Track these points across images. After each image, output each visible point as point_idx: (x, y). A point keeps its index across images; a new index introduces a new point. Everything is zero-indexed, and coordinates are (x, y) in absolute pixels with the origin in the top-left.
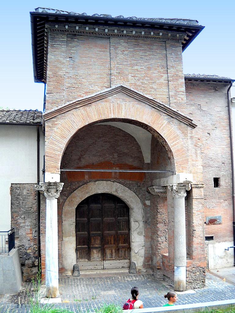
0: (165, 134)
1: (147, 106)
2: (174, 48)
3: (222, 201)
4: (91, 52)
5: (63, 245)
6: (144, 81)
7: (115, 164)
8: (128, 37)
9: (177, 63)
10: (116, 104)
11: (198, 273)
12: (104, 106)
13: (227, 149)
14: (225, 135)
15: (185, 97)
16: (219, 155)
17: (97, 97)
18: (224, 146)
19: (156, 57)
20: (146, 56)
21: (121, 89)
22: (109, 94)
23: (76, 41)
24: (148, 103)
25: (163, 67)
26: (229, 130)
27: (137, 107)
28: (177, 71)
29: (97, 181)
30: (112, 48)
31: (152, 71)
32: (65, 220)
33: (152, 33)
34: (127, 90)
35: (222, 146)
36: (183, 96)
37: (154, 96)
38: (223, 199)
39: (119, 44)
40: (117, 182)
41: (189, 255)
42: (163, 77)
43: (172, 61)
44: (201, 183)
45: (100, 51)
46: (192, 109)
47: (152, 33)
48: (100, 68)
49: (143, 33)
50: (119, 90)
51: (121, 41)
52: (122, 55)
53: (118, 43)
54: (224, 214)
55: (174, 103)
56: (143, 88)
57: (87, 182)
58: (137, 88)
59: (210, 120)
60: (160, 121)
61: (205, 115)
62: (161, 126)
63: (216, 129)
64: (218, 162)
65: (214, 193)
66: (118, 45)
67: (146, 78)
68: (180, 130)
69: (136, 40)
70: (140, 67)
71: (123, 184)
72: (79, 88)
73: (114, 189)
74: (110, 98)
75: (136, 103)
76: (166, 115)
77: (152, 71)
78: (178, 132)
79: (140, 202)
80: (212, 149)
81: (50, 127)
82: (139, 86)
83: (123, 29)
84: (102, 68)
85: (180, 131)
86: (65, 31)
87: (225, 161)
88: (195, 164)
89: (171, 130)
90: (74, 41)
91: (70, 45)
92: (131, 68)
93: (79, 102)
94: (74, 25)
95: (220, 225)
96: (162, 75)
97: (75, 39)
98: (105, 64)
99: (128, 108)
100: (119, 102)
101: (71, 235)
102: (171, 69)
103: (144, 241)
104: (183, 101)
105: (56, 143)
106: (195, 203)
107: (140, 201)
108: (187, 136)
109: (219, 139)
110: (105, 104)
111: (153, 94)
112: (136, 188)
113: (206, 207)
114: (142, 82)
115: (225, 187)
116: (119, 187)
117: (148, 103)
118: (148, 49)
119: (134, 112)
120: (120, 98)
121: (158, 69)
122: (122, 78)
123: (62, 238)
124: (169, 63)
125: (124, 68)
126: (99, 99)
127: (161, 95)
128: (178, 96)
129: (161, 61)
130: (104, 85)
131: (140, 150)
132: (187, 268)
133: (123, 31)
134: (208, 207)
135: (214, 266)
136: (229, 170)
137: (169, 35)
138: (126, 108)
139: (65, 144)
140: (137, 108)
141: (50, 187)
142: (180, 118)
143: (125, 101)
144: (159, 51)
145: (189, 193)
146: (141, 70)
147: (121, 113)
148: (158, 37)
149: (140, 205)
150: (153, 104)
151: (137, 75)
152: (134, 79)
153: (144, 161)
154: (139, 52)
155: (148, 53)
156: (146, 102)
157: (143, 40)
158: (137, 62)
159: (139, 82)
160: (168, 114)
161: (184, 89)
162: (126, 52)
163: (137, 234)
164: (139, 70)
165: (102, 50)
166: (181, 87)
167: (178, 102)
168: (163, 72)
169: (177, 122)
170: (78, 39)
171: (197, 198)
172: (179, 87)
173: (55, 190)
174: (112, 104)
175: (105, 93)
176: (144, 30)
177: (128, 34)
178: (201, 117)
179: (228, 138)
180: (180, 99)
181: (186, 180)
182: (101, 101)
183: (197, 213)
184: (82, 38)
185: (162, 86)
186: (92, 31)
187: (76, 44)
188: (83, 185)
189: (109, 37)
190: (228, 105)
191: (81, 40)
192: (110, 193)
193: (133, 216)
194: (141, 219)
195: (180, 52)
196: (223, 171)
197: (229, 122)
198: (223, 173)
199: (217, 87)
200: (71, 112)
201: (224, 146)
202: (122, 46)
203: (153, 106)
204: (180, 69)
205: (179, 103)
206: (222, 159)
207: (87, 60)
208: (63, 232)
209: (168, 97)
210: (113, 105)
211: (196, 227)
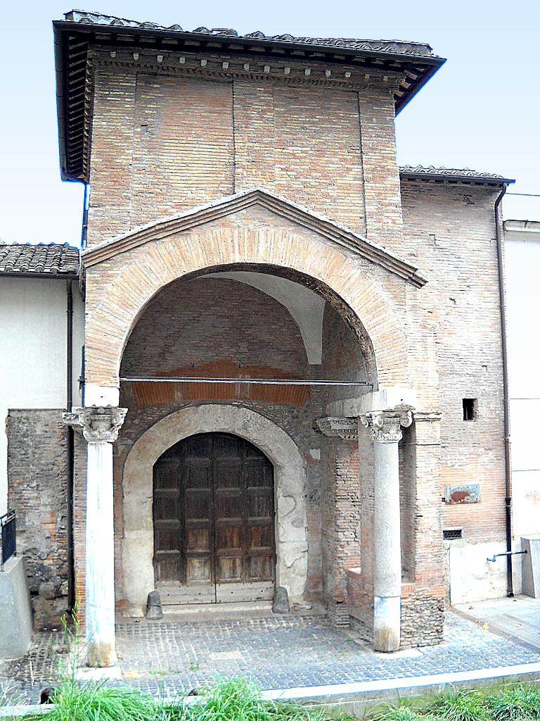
3: (481, 452)
6: (307, 180)
7: (242, 366)
9: (384, 139)
10: (246, 232)
12: (219, 236)
20: (313, 123)
21: (258, 197)
24: (317, 230)
26: (498, 293)
36: (398, 215)
40: (246, 407)
41: (408, 571)
43: (372, 137)
49: (308, 72)
57: (180, 408)
66: (251, 98)
70: (300, 149)
72: (162, 194)
73: (240, 423)
74: (233, 217)
76: (357, 256)
78: (385, 296)
81: (97, 282)
82: (298, 191)
84: (215, 150)
86: (133, 64)
89: (368, 291)
92: (281, 150)
94: (153, 51)
96: (349, 166)
100: (251, 227)
101: (143, 527)
113: (446, 464)
116: (251, 418)
117: (317, 230)
128: (386, 214)
130: (220, 189)
131: (297, 336)
134: (450, 465)
138: (269, 241)
141: (97, 417)
145: (408, 432)
149: (299, 459)
151: (292, 167)
156: (313, 228)
160: (361, 253)
161: (397, 199)
173: (108, 425)
177: (274, 75)
180: (388, 220)
181: (400, 403)
182: (211, 224)
185: (349, 192)
186: (194, 65)
187: (157, 95)
189: (231, 79)
192: (230, 431)
200: (146, 248)
202: (260, 101)
207: (181, 132)
210: (239, 233)
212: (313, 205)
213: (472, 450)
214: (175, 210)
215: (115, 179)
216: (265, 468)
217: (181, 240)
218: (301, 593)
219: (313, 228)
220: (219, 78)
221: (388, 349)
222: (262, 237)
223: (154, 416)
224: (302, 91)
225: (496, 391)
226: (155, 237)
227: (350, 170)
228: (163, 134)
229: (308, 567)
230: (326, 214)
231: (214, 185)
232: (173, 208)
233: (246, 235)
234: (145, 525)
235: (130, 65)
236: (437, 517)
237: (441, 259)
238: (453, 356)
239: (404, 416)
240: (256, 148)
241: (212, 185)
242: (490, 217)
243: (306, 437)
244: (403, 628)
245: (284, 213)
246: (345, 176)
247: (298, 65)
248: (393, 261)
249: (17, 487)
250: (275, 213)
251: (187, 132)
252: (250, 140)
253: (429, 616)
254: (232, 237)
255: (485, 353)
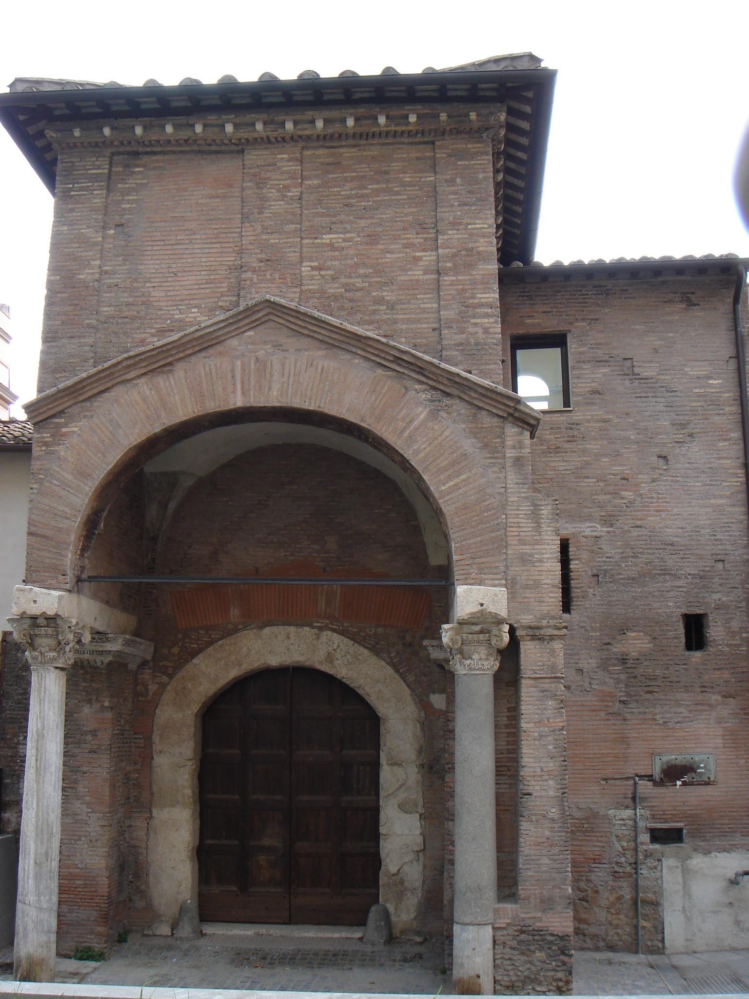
0: (417, 452)
1: (357, 361)
2: (461, 160)
3: (717, 700)
4: (183, 202)
5: (152, 835)
6: (352, 281)
7: (328, 569)
8: (301, 144)
9: (473, 208)
10: (253, 362)
11: (538, 954)
12: (214, 371)
13: (737, 509)
14: (726, 458)
15: (496, 322)
16: (703, 531)
17: (190, 341)
18: (720, 501)
19: (398, 197)
20: (362, 196)
21: (269, 310)
22: (227, 330)
23: (139, 172)
24: (360, 352)
25: (422, 227)
26: (741, 442)
27: (323, 368)
28: (471, 235)
29: (265, 627)
30: (251, 181)
31: (381, 247)
32: (161, 752)
33: (382, 120)
34: (288, 312)
35: (713, 501)
36: (492, 320)
37: (384, 327)
38: (719, 693)
39: (271, 168)
40: (334, 630)
41: (507, 882)
42: (421, 263)
43: (453, 206)
44: (552, 622)
45: (212, 197)
46: (600, 376)
47: (382, 120)
48: (208, 251)
49: (350, 122)
50: (261, 315)
51: (279, 156)
52: (282, 203)
53: (269, 165)
54: (724, 747)
55: (455, 345)
56: (348, 305)
57: (236, 631)
58: (330, 306)
59: (670, 409)
60: (401, 410)
61: (650, 395)
62: (405, 428)
63: (688, 439)
64: (701, 557)
65: (686, 669)
66: (268, 171)
67: (361, 271)
68: (476, 437)
69: (333, 147)
70: (342, 236)
71: (353, 638)
72: (140, 318)
73: (321, 654)
74: (234, 342)
75: (320, 353)
76: (424, 387)
77: (381, 247)
78: (468, 445)
79: (409, 698)
80: (675, 511)
81: (46, 444)
82: (336, 297)
83: (283, 117)
84: (214, 250)
85: (474, 440)
86: (104, 143)
87: (726, 554)
88: (531, 555)
89: (440, 439)
90: (133, 172)
91: (120, 186)
92: (311, 241)
93: (132, 361)
94: (128, 122)
95: (709, 788)
96: (417, 254)
97: (137, 166)
98: (224, 235)
99: (292, 371)
100: (261, 354)
101: (178, 802)
102: (450, 232)
103: (421, 834)
104: (491, 336)
105: (63, 493)
106: (527, 690)
107: (412, 695)
108: (500, 455)
109: (702, 475)
110: (216, 365)
111: (381, 321)
112: (398, 653)
113: (655, 719)
114: (347, 284)
115: (726, 649)
116: (338, 646)
117: (360, 352)
118: (372, 173)
119: (311, 384)
120: (265, 342)
121: (403, 236)
122: (277, 276)
123: (151, 811)
124: (444, 212)
125: (286, 243)
126: (197, 349)
127: (409, 321)
128: (473, 321)
129: (415, 210)
130: (220, 304)
131: (413, 523)
132: (499, 933)
133: (283, 124)
134: (661, 722)
135: (687, 940)
136: (744, 588)
137: (441, 118)
138: (286, 373)
139: (87, 495)
140: (322, 372)
141: (37, 632)
142: (473, 395)
143: (283, 350)
144: (411, 177)
145: (510, 655)
146: (343, 244)
147: (270, 389)
148: (404, 128)
149: (411, 709)
150: (376, 353)
151: (329, 263)
152: (319, 277)
153: (426, 557)
154: (340, 186)
155: (370, 187)
156: (354, 350)
157: (354, 146)
158: (334, 219)
159: (336, 285)
160: (430, 382)
161: (493, 295)
162: (293, 190)
163: (396, 807)
164: (337, 245)
165: (219, 191)
166: (484, 289)
167: (472, 341)
168: (420, 243)
169: (463, 411)
170: (144, 166)
171: (538, 676)
172: (476, 291)
173: (52, 642)
174: (239, 363)
175: (215, 328)
176: (352, 111)
177: (300, 133)
178: (634, 399)
179: (740, 471)
180: (476, 329)
181: (480, 608)
182: (203, 354)
183: (538, 730)
184: (157, 161)
185: (417, 292)
186: (185, 134)
187: (138, 181)
188: (221, 639)
189: (240, 147)
190: (738, 351)
191: (154, 169)
192: (308, 664)
193: (385, 745)
194: (414, 757)
195: (484, 172)
196: (720, 589)
197: (740, 411)
198: (718, 596)
199: (693, 293)
200: (113, 393)
201: (720, 501)
202: (282, 173)
203: (378, 360)
204: (483, 228)
205: (476, 344)
206: (714, 544)
207: (168, 229)
208: (155, 788)
209: (435, 326)
210: (243, 364)
211: (533, 783)
212: (359, 316)
213: (700, 697)
214: (156, 339)
215: (76, 302)
216: (366, 723)
217: (161, 381)
218: (413, 915)
219: (354, 350)
220: (223, 148)
221: (472, 527)
222: (277, 366)
223: (199, 642)
224: (348, 153)
225: (741, 602)
226: (123, 378)
227: (419, 259)
228: (144, 234)
229: (424, 876)
230: (379, 328)
231: (212, 300)
232: (153, 335)
233: (252, 366)
234: (181, 799)
235: (100, 144)
236: (557, 797)
237: (643, 395)
238: (663, 547)
239: (495, 631)
240: (272, 241)
241: (208, 301)
242: (725, 323)
243: (424, 675)
244: (498, 978)
245: (309, 330)
246: (410, 270)
247: (334, 113)
248: (479, 390)
249: (12, 739)
250: (296, 331)
251: (177, 229)
252: (265, 231)
253: (544, 962)
254: (233, 371)
255: (720, 540)
